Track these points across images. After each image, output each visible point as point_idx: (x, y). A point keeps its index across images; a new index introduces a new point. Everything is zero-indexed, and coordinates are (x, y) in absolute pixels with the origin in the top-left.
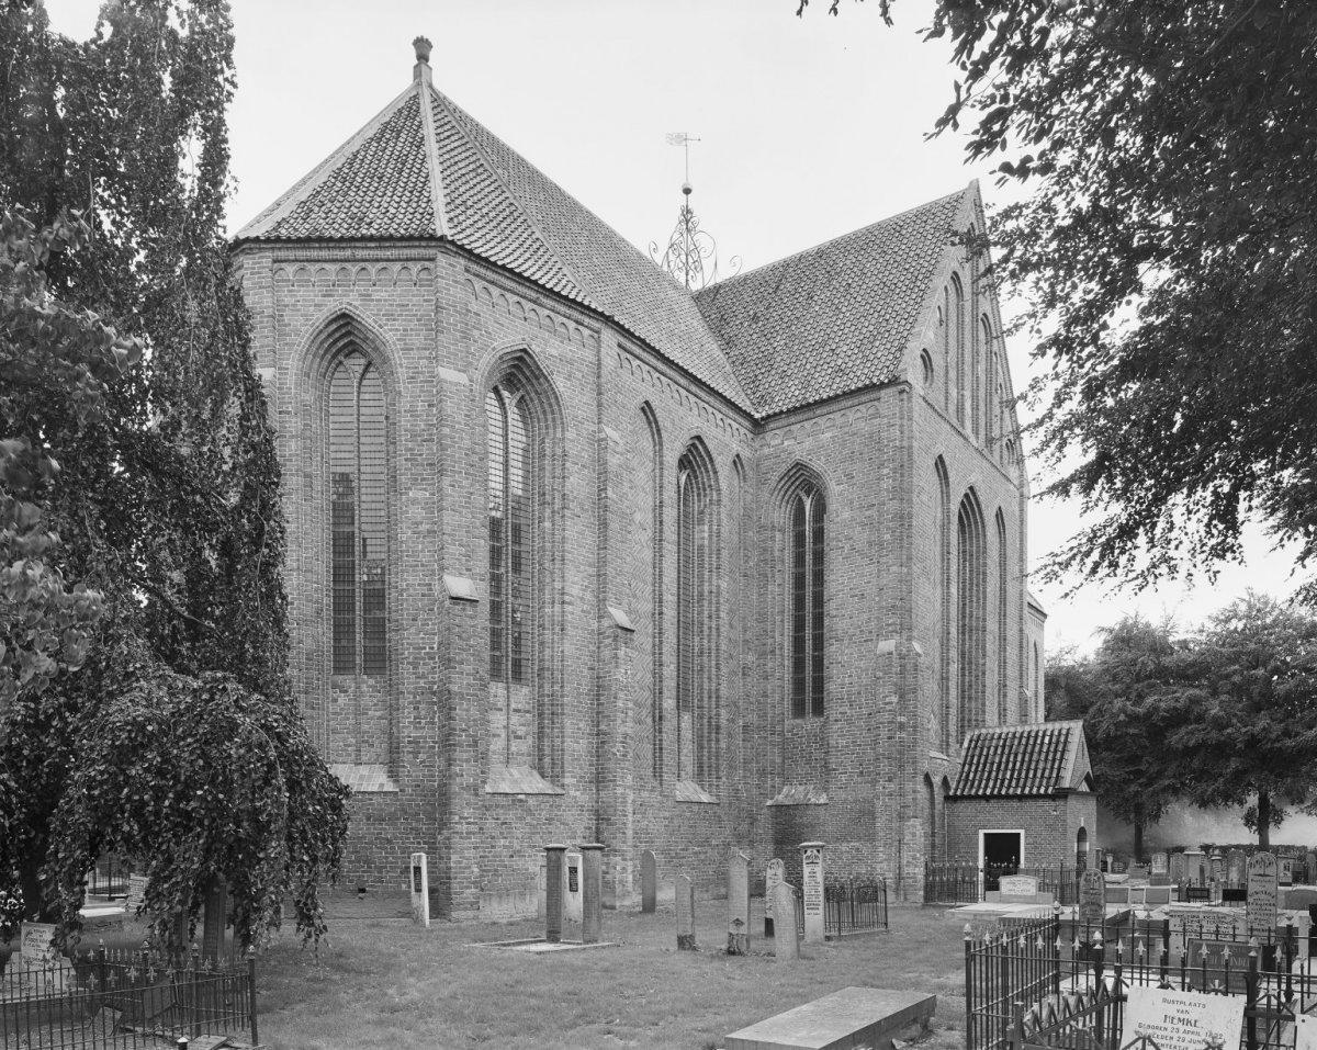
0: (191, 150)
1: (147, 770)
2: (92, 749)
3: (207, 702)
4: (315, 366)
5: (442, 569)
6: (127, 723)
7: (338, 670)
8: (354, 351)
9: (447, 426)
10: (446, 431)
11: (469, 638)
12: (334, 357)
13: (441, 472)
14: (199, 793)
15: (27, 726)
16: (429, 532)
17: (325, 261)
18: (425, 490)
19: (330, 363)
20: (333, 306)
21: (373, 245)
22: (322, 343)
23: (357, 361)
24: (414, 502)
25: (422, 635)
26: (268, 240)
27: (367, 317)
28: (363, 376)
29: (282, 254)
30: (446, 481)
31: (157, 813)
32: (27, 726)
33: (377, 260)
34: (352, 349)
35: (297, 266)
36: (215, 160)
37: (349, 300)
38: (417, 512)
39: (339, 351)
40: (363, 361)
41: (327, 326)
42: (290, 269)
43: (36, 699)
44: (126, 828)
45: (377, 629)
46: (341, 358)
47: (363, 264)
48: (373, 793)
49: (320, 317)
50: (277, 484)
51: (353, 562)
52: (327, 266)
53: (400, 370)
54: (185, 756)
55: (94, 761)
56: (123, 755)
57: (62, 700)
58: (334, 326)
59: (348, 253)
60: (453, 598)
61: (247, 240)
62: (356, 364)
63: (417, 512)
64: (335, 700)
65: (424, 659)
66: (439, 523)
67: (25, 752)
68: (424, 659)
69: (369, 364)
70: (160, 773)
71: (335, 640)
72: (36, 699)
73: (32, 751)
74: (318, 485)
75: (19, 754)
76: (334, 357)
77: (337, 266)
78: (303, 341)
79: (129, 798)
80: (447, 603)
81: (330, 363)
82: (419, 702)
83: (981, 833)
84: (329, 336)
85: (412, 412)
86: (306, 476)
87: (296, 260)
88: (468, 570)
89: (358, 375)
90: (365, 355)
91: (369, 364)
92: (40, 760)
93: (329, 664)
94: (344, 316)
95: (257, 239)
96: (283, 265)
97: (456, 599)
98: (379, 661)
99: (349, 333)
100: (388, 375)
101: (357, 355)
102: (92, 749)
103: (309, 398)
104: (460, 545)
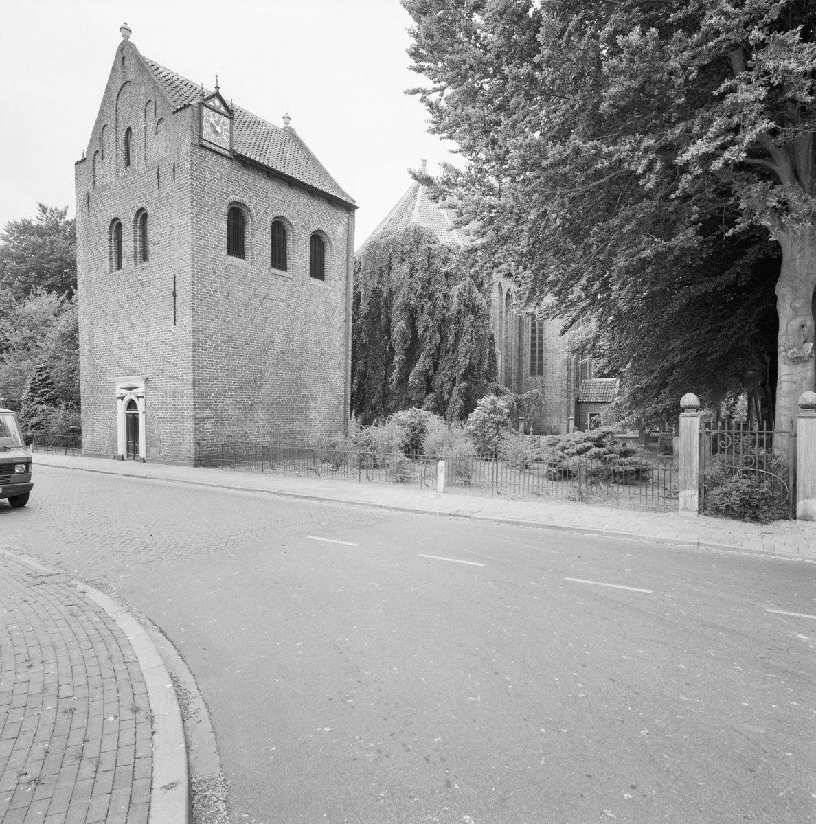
83: (589, 414)
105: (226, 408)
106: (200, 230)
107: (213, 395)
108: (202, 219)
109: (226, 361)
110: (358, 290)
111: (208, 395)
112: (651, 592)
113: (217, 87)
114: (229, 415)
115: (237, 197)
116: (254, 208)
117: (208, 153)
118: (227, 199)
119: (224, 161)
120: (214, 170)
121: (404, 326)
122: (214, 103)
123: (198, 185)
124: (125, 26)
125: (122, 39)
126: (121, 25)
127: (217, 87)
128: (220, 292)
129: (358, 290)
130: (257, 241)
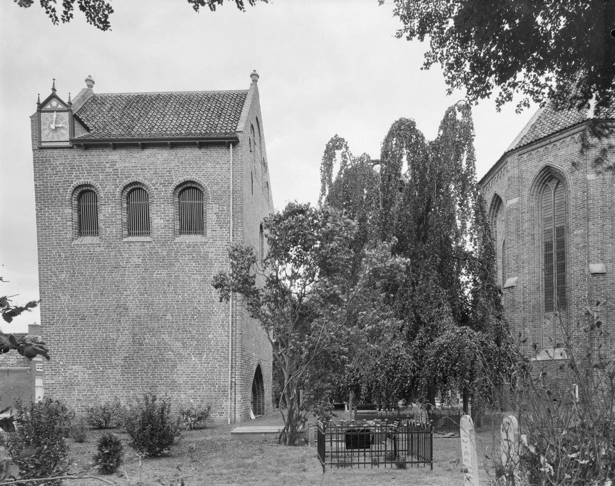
0: (464, 157)
1: (444, 358)
2: (430, 353)
3: (460, 336)
4: (536, 190)
5: (589, 262)
6: (439, 345)
7: (547, 311)
8: (552, 178)
9: (590, 199)
10: (590, 201)
11: (601, 290)
12: (544, 184)
13: (588, 220)
14: (457, 364)
15: (420, 347)
16: (583, 247)
17: (539, 148)
18: (581, 229)
19: (542, 187)
20: (542, 165)
21: (558, 134)
22: (538, 181)
23: (554, 182)
24: (576, 235)
25: (580, 291)
26: (516, 149)
27: (556, 165)
28: (556, 188)
29: (521, 152)
30: (591, 223)
31: (447, 371)
32: (420, 347)
33: (560, 139)
34: (551, 178)
35: (527, 154)
36: (471, 160)
37: (550, 160)
38: (578, 240)
39: (546, 181)
40: (556, 181)
41: (539, 174)
42: (525, 156)
43: (422, 339)
44: (439, 375)
45: (562, 293)
46: (547, 183)
47: (554, 143)
48: (559, 360)
49: (537, 171)
50: (494, 257)
51: (552, 265)
52: (539, 150)
53: (570, 181)
54: (454, 353)
55: (431, 356)
56: (439, 354)
57: (429, 338)
58: (543, 172)
59: (548, 141)
60: (592, 274)
61: (509, 151)
62: (552, 185)
63: (578, 240)
64: (545, 323)
65: (581, 302)
66: (587, 242)
67: (419, 354)
68: (581, 302)
69: (559, 182)
70: (448, 359)
71: (545, 298)
72: (422, 339)
73: (421, 354)
74: (536, 237)
75: (417, 355)
76: (544, 184)
77: (544, 148)
78: (530, 183)
79: (440, 367)
80: (590, 277)
81: (542, 187)
82: (579, 320)
84: (541, 176)
85: (576, 198)
86: (532, 235)
87: (527, 152)
88: (601, 260)
89: (554, 188)
90: (557, 178)
91: (559, 182)
92: (423, 356)
93: (543, 308)
94: (547, 167)
95: (512, 150)
96: (522, 156)
97: (594, 274)
98: (564, 303)
99: (549, 173)
100: (565, 186)
101: (554, 179)
102: (430, 353)
103: (533, 204)
104: (598, 250)
105: (76, 374)
106: (45, 222)
107: (61, 363)
108: (46, 212)
109: (74, 332)
110: (519, 83)
111: (57, 363)
112: (586, 8)
113: (54, 89)
114: (78, 381)
115: (82, 180)
116: (100, 185)
117: (49, 151)
118: (70, 186)
119: (66, 152)
120: (56, 164)
121: (497, 284)
122: (58, 105)
123: (41, 183)
124: (89, 78)
125: (52, 93)
126: (87, 77)
127: (54, 89)
128: (66, 271)
129: (519, 83)
130: (104, 215)
